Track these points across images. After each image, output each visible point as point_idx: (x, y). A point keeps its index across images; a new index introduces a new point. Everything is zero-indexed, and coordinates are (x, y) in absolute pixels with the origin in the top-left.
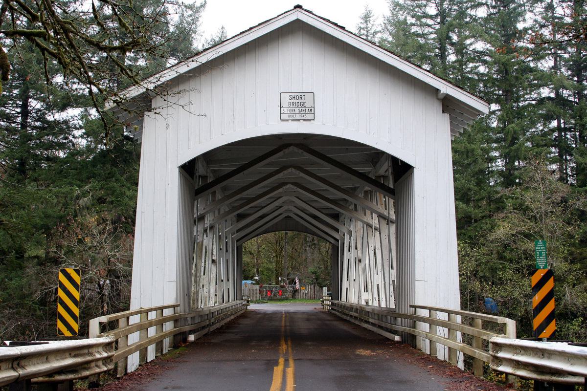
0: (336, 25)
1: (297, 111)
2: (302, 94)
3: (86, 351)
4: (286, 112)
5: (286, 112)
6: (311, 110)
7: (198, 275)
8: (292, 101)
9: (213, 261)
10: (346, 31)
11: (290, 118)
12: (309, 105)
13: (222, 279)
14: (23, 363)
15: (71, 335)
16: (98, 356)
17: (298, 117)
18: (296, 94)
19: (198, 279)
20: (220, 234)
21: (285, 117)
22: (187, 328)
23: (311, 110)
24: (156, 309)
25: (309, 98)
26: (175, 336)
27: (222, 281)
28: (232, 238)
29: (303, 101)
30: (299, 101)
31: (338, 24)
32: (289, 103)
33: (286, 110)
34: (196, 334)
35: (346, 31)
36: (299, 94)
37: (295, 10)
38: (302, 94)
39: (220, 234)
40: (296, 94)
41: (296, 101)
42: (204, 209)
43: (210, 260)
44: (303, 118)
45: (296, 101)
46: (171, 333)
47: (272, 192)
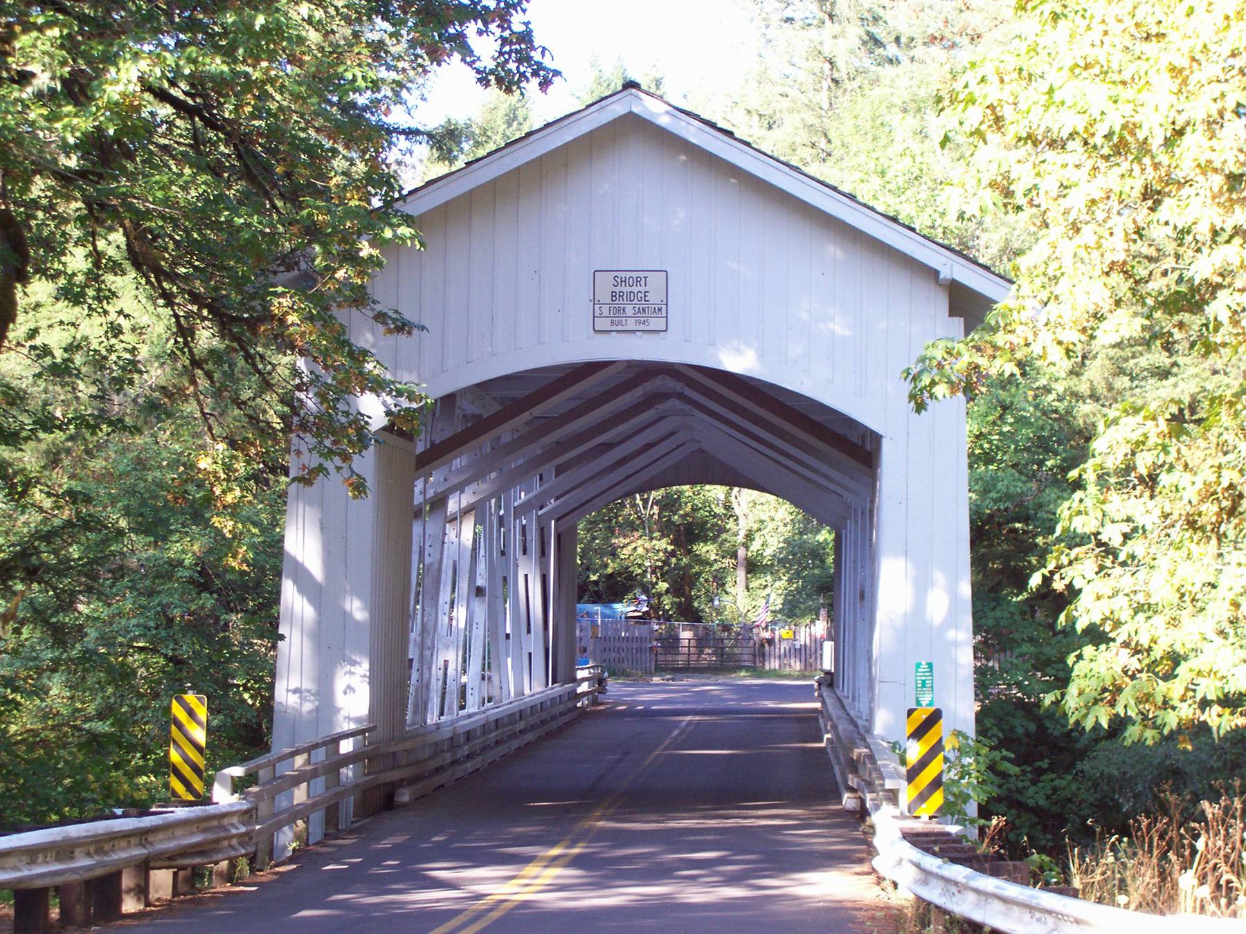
0: (712, 125)
1: (629, 310)
2: (641, 274)
3: (215, 823)
4: (606, 313)
5: (606, 313)
6: (661, 309)
7: (429, 643)
8: (618, 289)
9: (479, 592)
10: (736, 139)
11: (614, 328)
12: (654, 298)
13: (508, 631)
14: (151, 838)
15: (191, 798)
16: (234, 831)
17: (631, 325)
18: (628, 274)
19: (428, 653)
20: (502, 513)
21: (603, 324)
22: (394, 775)
23: (660, 310)
24: (325, 744)
25: (655, 282)
26: (364, 792)
27: (508, 636)
28: (539, 517)
29: (643, 289)
30: (635, 289)
31: (719, 125)
32: (613, 294)
33: (605, 309)
34: (415, 787)
35: (736, 139)
36: (635, 275)
37: (625, 93)
38: (641, 274)
39: (502, 513)
40: (628, 274)
41: (628, 289)
42: (445, 480)
43: (463, 585)
44: (642, 327)
45: (628, 289)
46: (356, 786)
47: (623, 422)
